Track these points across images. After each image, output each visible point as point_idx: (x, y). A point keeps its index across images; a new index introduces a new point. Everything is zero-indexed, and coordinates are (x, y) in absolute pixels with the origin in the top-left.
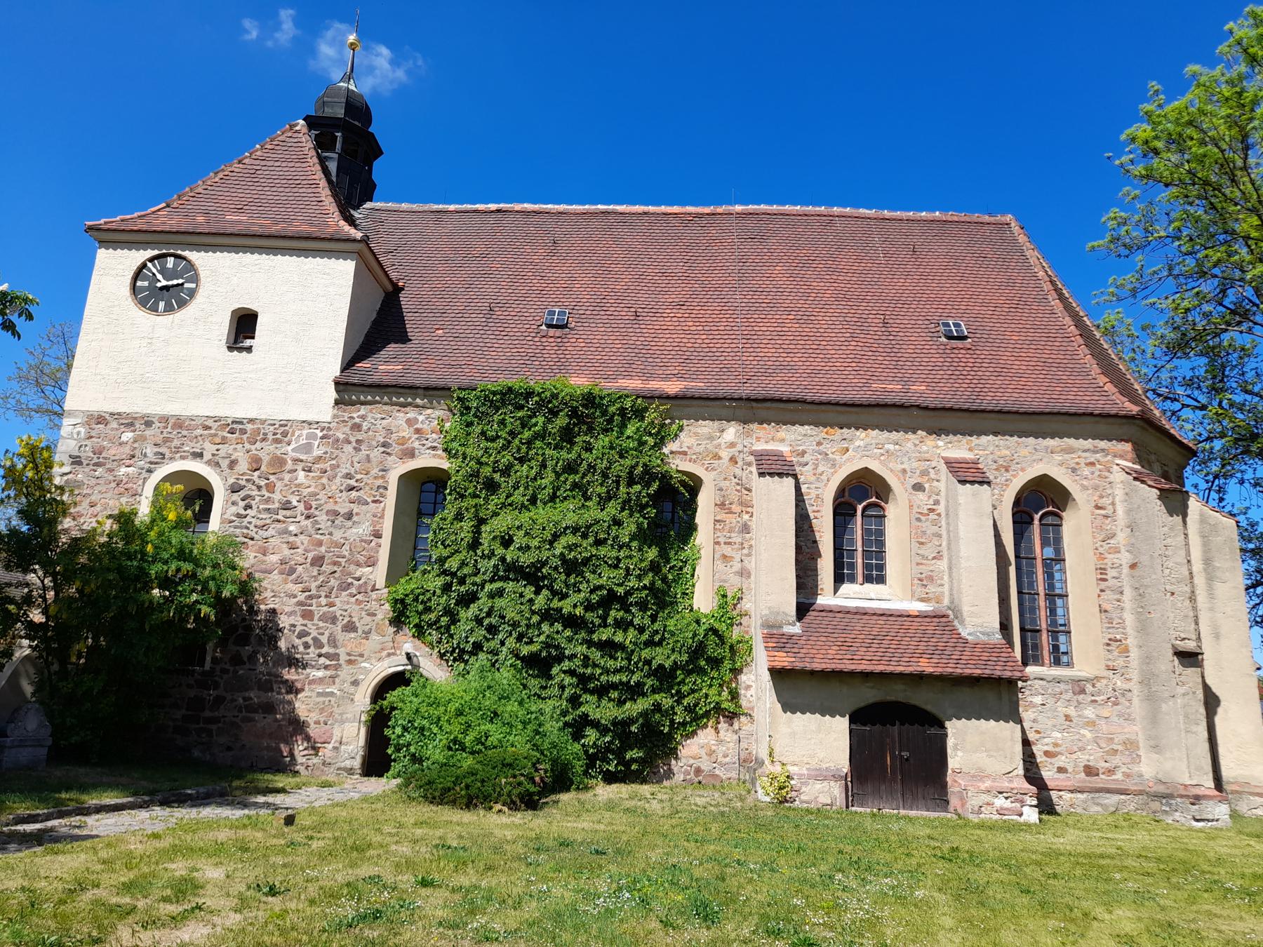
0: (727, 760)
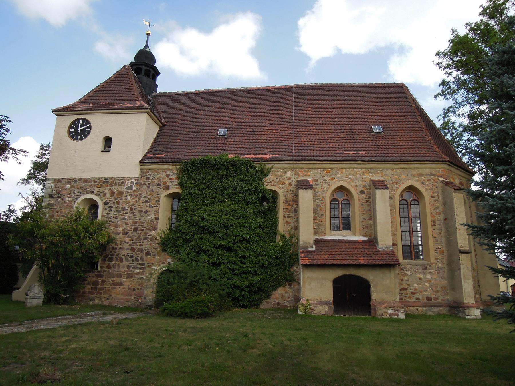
0: (290, 299)
